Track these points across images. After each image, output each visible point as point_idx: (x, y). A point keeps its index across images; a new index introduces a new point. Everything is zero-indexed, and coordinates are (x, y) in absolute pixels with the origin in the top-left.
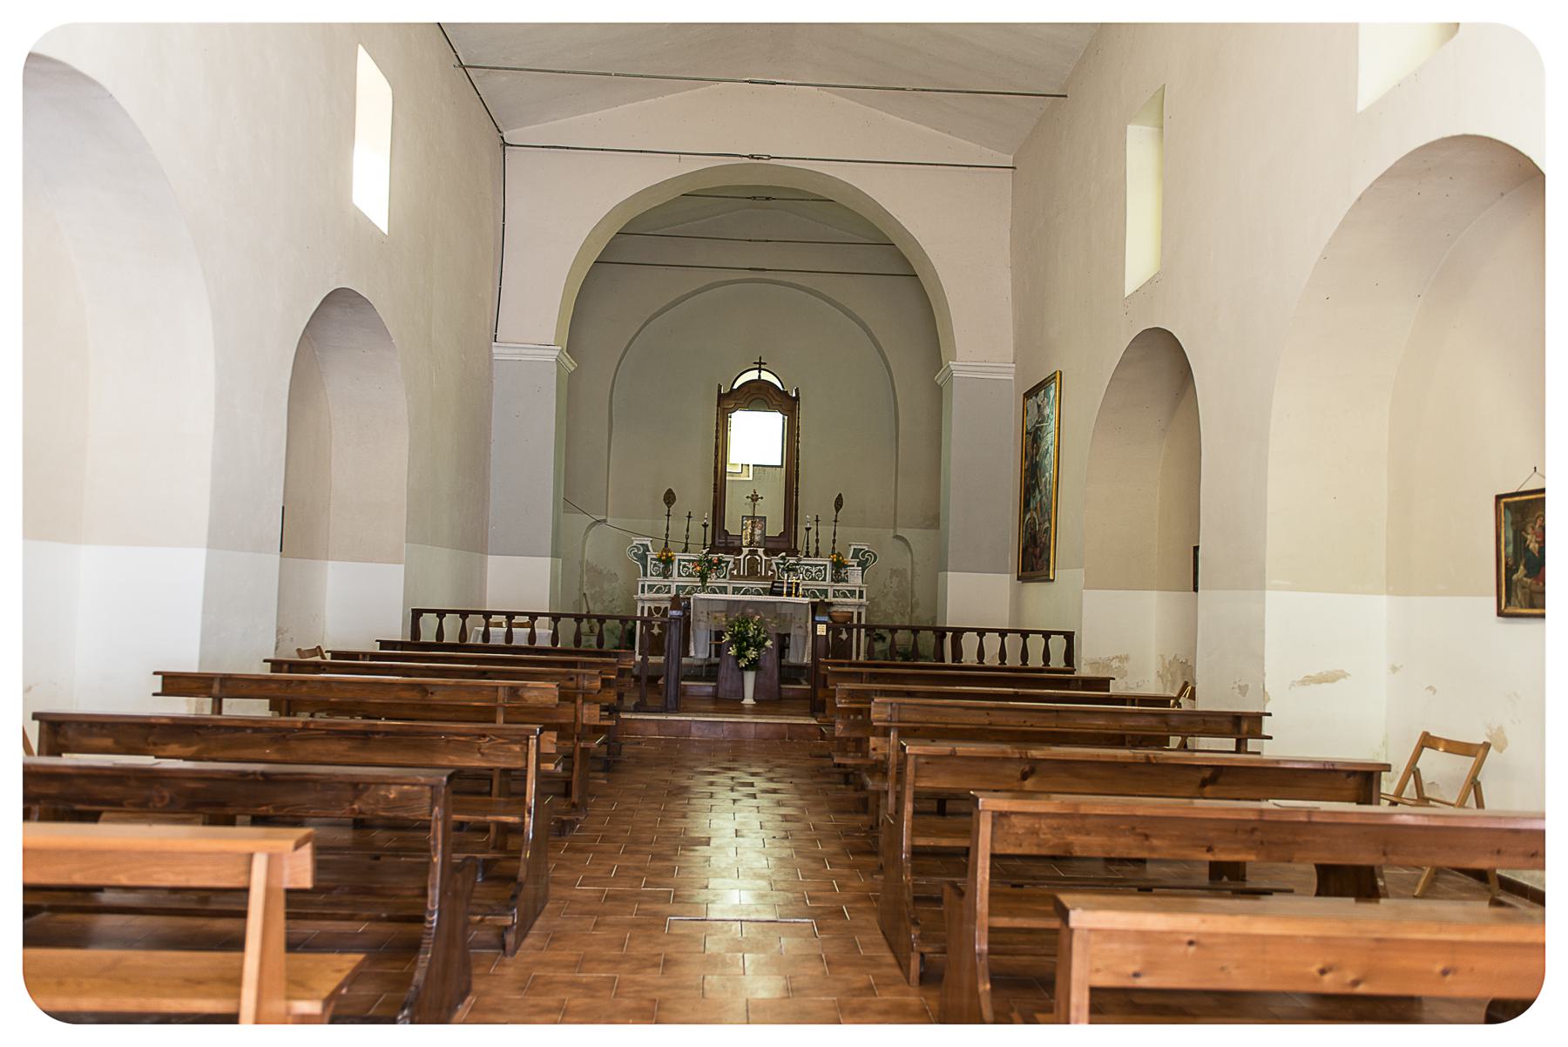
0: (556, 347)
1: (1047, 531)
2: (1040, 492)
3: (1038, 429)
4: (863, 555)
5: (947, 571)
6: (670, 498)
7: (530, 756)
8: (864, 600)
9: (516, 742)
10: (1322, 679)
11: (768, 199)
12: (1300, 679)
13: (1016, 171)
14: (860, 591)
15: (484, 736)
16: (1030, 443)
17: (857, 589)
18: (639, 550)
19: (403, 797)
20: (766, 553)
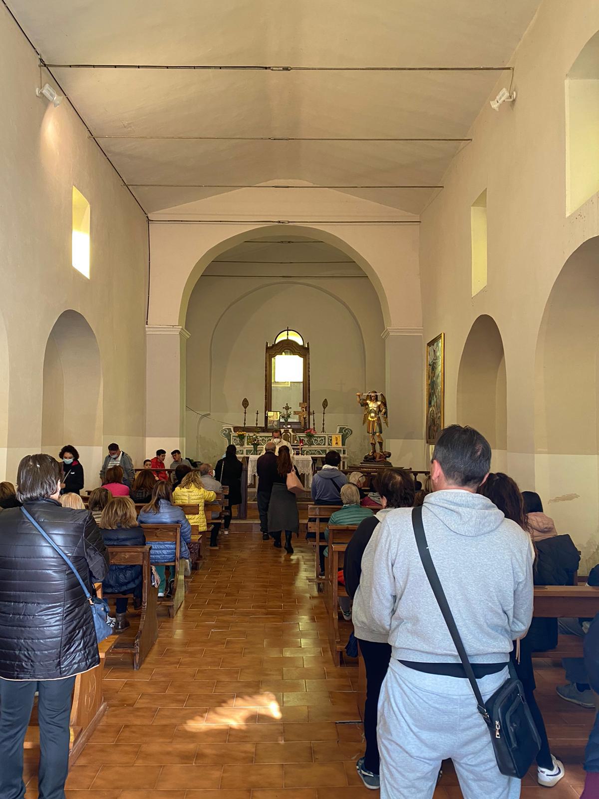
0: (179, 327)
1: (439, 418)
2: (436, 397)
3: (434, 363)
4: (345, 432)
5: (146, 437)
6: (245, 403)
7: (177, 537)
8: (346, 455)
9: (171, 531)
10: (565, 498)
11: (289, 242)
12: (554, 499)
13: (421, 223)
14: (343, 450)
15: (158, 529)
16: (431, 371)
17: (342, 449)
18: (226, 431)
19: (131, 557)
20: (293, 431)
